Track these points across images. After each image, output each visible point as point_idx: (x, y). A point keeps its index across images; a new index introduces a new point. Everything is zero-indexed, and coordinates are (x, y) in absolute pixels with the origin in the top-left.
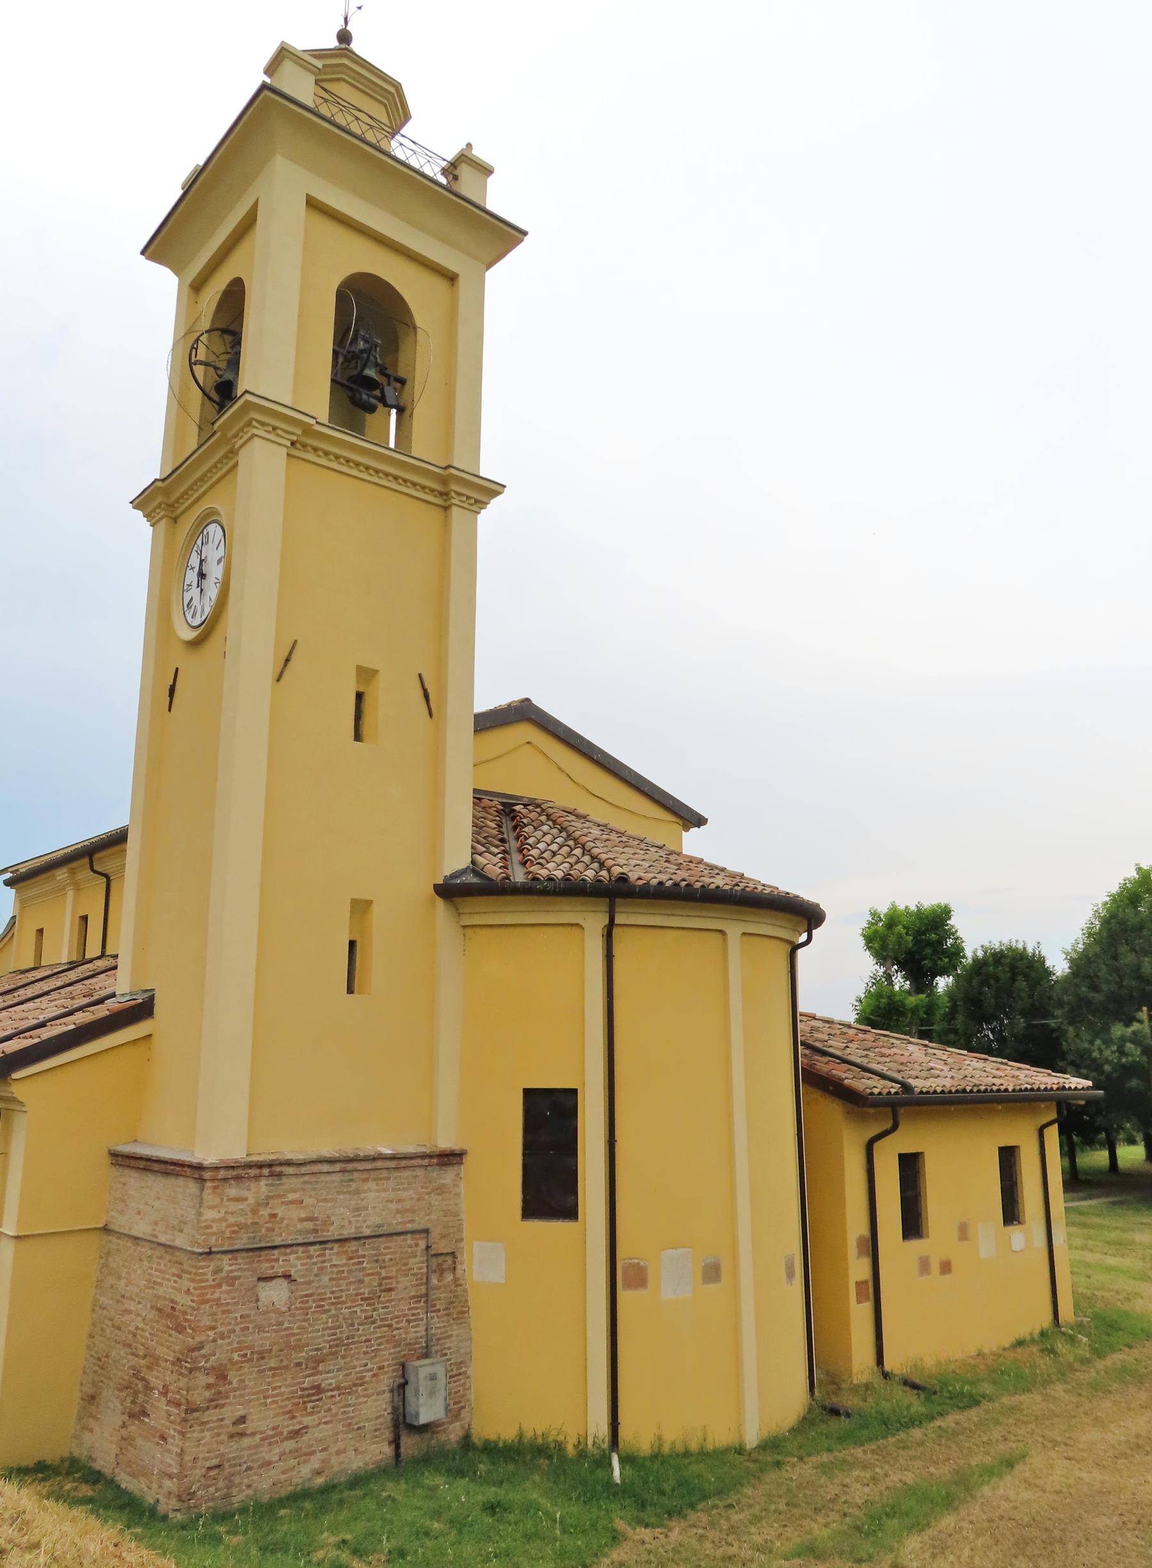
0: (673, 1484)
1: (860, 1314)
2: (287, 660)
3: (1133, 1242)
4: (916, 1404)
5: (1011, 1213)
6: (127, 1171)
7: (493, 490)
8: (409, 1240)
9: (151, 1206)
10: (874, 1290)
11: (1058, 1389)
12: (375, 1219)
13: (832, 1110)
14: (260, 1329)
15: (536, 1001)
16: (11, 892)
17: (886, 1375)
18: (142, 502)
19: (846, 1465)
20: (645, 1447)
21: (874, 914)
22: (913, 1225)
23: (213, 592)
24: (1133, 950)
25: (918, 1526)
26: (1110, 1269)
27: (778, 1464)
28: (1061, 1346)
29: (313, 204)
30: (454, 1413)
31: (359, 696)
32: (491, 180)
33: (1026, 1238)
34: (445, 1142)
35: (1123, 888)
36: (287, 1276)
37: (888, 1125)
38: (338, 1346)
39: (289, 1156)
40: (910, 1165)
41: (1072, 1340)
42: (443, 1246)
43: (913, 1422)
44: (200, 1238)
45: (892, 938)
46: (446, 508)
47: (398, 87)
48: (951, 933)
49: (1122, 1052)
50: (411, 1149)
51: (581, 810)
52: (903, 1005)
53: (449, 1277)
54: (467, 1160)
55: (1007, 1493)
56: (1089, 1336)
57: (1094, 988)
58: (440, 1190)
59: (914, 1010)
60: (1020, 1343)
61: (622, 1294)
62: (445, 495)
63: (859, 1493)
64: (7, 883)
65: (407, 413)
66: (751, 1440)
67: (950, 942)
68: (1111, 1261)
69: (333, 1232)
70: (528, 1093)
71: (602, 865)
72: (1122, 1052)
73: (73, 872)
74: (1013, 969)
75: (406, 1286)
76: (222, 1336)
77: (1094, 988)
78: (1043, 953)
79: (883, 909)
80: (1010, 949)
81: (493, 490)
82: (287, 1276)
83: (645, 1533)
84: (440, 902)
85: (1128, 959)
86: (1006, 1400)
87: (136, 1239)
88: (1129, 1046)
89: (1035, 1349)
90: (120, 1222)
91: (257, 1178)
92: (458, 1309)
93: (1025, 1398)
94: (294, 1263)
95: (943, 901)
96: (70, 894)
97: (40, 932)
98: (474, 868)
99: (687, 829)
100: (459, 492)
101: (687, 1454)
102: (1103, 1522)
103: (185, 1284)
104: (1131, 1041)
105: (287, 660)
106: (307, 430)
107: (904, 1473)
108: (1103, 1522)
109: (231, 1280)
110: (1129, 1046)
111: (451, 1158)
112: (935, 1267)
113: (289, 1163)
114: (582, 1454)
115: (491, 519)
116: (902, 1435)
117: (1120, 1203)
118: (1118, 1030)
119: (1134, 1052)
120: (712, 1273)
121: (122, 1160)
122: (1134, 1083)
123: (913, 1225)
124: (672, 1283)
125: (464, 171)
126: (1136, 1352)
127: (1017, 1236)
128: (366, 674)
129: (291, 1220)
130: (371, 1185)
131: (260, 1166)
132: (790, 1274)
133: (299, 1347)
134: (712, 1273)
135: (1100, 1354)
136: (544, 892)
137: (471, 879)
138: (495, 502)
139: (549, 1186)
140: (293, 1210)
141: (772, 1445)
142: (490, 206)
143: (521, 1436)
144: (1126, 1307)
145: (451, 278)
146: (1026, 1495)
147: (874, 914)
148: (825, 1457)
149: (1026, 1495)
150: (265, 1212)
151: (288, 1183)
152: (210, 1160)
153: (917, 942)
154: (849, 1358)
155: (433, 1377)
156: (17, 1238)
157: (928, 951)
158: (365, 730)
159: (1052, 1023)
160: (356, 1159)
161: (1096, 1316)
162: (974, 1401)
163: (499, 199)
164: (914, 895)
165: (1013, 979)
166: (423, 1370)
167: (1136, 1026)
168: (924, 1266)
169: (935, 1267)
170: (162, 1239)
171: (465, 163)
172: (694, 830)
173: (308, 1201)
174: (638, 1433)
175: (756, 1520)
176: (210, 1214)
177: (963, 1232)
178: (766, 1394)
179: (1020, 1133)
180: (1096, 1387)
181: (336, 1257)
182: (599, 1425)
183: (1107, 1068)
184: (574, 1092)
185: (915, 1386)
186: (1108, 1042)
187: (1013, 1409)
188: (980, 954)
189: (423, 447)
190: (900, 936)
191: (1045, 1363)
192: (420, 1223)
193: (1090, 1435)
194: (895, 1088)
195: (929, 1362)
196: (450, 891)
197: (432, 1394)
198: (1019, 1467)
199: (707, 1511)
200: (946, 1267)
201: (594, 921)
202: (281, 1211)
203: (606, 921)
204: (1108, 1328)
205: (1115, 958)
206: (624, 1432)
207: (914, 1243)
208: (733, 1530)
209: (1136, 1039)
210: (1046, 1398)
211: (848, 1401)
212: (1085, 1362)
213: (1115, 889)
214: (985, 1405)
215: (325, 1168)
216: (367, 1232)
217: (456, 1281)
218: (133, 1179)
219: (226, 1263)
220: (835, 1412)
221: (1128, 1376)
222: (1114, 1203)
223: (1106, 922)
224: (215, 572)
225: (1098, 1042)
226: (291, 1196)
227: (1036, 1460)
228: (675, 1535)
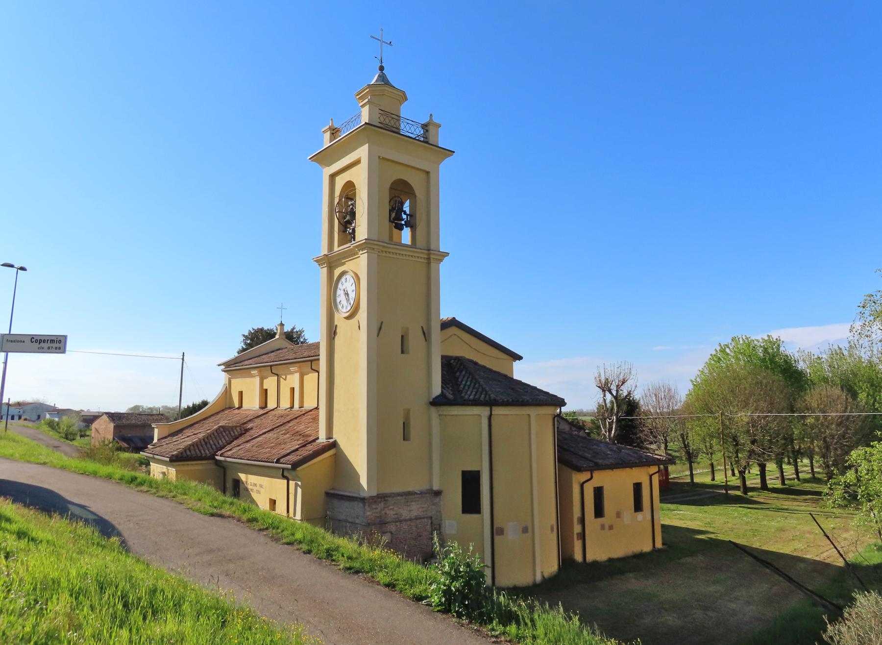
2: (380, 329)
5: (638, 507)
10: (583, 536)
12: (415, 514)
33: (643, 517)
34: (436, 488)
37: (589, 477)
61: (497, 538)
70: (65, 337)
73: (260, 371)
98: (443, 395)
105: (380, 329)
111: (438, 493)
112: (607, 527)
120: (525, 530)
123: (599, 512)
124: (512, 535)
127: (640, 516)
131: (381, 498)
132: (552, 530)
134: (525, 530)
139: (471, 504)
142: (515, 378)
168: (603, 527)
169: (607, 527)
176: (368, 513)
177: (618, 515)
184: (478, 472)
189: (421, 242)
192: (430, 515)
196: (436, 402)
202: (388, 512)
207: (599, 520)
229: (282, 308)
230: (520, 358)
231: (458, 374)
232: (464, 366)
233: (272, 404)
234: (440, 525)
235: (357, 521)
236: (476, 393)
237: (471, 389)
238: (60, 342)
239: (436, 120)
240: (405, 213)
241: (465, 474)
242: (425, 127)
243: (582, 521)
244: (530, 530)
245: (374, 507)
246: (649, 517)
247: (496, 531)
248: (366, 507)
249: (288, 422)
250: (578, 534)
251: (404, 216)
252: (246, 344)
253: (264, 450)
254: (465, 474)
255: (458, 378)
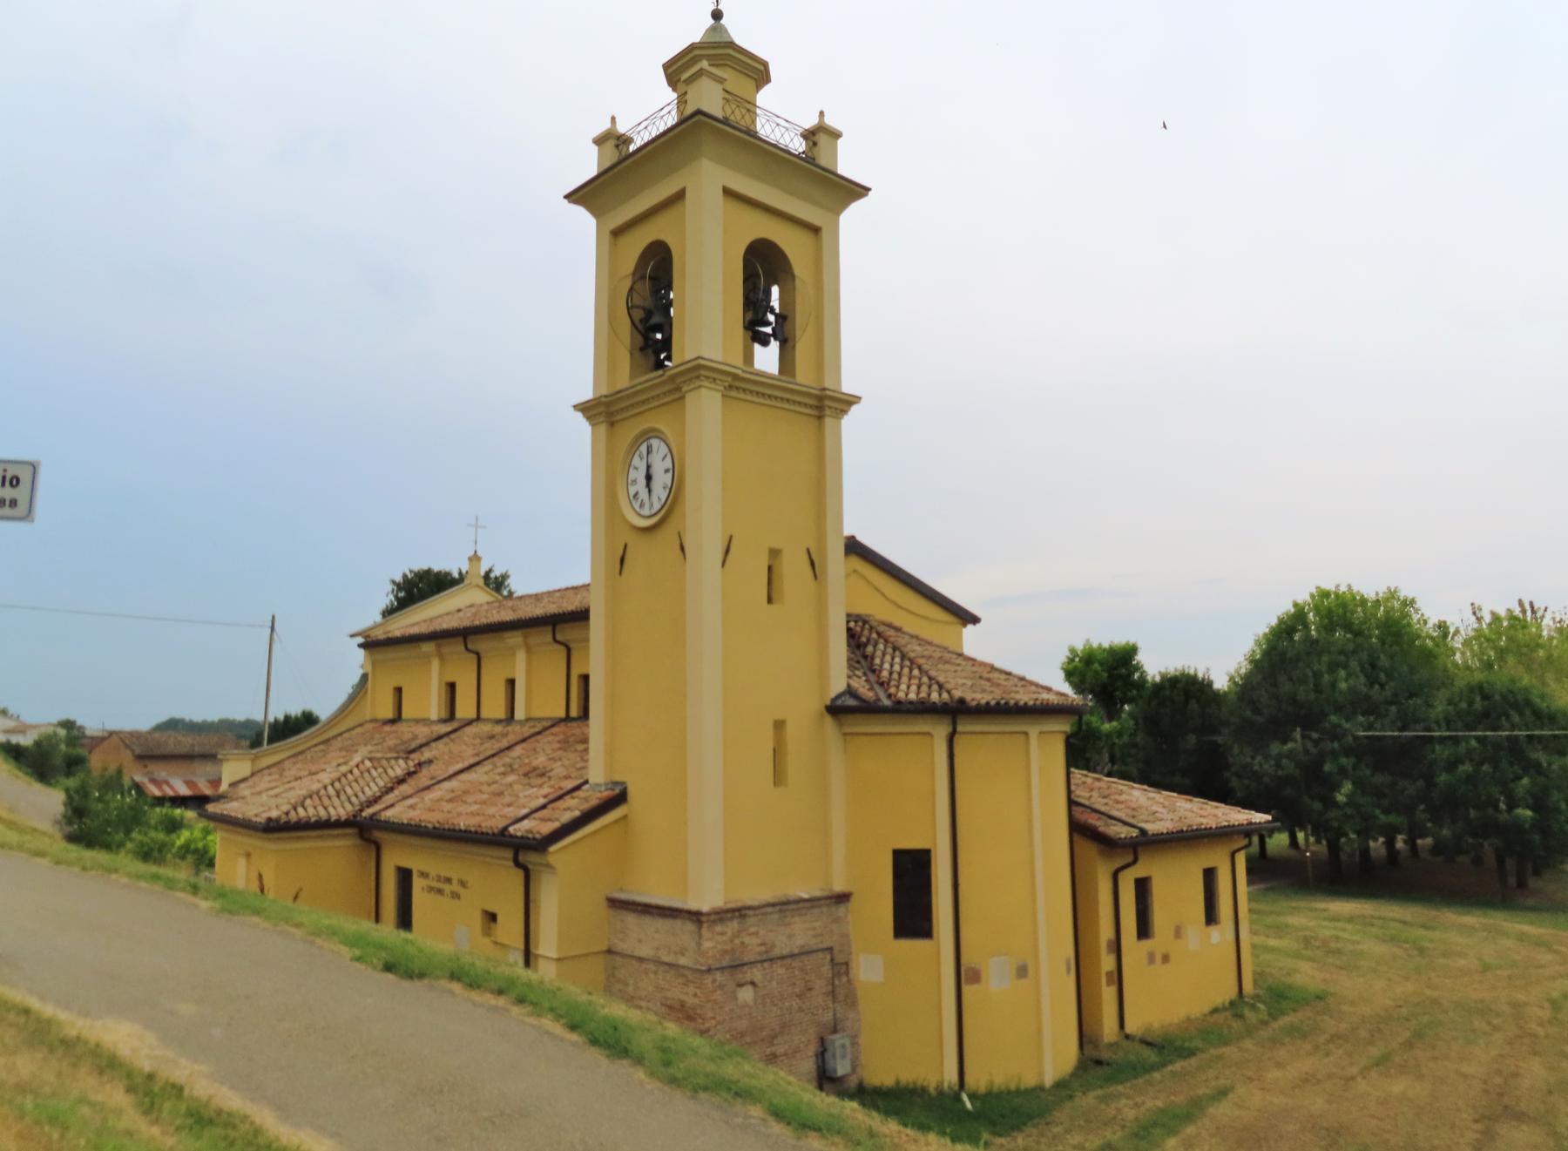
0: (1008, 1110)
1: (1108, 994)
2: (727, 551)
3: (1287, 926)
4: (1150, 1056)
5: (1211, 917)
6: (625, 913)
7: (849, 401)
8: (820, 955)
9: (644, 937)
10: (1118, 978)
11: (1248, 1043)
13: (1088, 849)
14: (740, 1017)
15: (903, 793)
16: (362, 652)
17: (1127, 1037)
18: (585, 409)
19: (1119, 1096)
20: (982, 1089)
21: (1072, 651)
22: (1144, 930)
23: (660, 493)
24: (1290, 679)
25: (1172, 1132)
26: (1272, 950)
27: (1071, 1097)
28: (1247, 1012)
29: (728, 192)
30: (854, 1068)
31: (770, 568)
32: (840, 142)
33: (1221, 934)
34: (839, 887)
35: (1281, 621)
36: (753, 984)
37: (1130, 859)
38: (785, 1027)
39: (749, 903)
40: (1142, 886)
41: (1253, 1007)
42: (840, 958)
43: (1154, 1068)
44: (702, 960)
45: (1089, 675)
46: (820, 418)
47: (765, 65)
48: (1138, 668)
49: (1278, 766)
50: (818, 893)
51: (897, 623)
52: (1099, 731)
53: (844, 979)
54: (853, 899)
55: (1222, 1111)
56: (1264, 1003)
57: (1257, 711)
58: (837, 920)
59: (1109, 735)
60: (1215, 1011)
61: (966, 989)
62: (820, 408)
63: (1130, 1114)
64: (360, 646)
65: (789, 344)
66: (1048, 1081)
67: (1136, 676)
68: (1272, 942)
69: (777, 952)
71: (941, 686)
72: (1278, 766)
73: (439, 646)
74: (1186, 691)
75: (820, 986)
76: (719, 1023)
77: (1257, 711)
78: (1212, 677)
79: (1079, 647)
80: (1183, 674)
81: (849, 401)
82: (753, 984)
83: (1002, 1140)
84: (828, 719)
85: (1286, 687)
86: (1213, 1051)
87: (641, 959)
88: (1285, 761)
89: (1228, 1014)
90: (621, 946)
91: (731, 919)
92: (851, 1000)
93: (1225, 1050)
94: (756, 974)
95: (1132, 641)
96: (435, 664)
97: (399, 691)
98: (850, 691)
99: (965, 625)
100: (827, 405)
101: (1009, 1092)
102: (1291, 1128)
103: (692, 989)
104: (1288, 757)
105: (727, 551)
106: (735, 377)
107: (1153, 1102)
108: (1291, 1128)
109: (721, 987)
110: (1285, 761)
111: (843, 898)
112: (1159, 958)
113: (750, 908)
114: (941, 1093)
115: (851, 424)
116: (1147, 1077)
117: (1272, 889)
118: (1275, 748)
119: (1289, 767)
120: (1022, 972)
121: (614, 903)
122: (1288, 791)
123: (1144, 930)
124: (996, 981)
125: (822, 139)
126: (1300, 1015)
128: (775, 553)
129: (752, 944)
130: (797, 919)
131: (733, 910)
132: (1069, 970)
133: (762, 1029)
135: (1274, 1017)
136: (908, 712)
137: (851, 702)
138: (854, 408)
139: (912, 917)
140: (753, 939)
141: (1060, 1085)
142: (841, 171)
143: (898, 1083)
144: (1288, 980)
145: (815, 230)
146: (1237, 1113)
147: (1072, 651)
148: (1100, 1092)
149: (1237, 1113)
150: (737, 941)
151: (751, 921)
152: (705, 908)
153: (1110, 676)
154: (1101, 1026)
155: (843, 1046)
156: (559, 960)
157: (1119, 683)
158: (774, 596)
159: (1220, 739)
160: (788, 903)
161: (1270, 989)
162: (1192, 1053)
163: (848, 164)
164: (1107, 637)
165: (1187, 702)
166: (838, 1040)
167: (1290, 745)
168: (1151, 958)
169: (1159, 958)
170: (666, 959)
171: (819, 135)
172: (970, 627)
173: (762, 932)
174: (978, 1079)
175: (1068, 1131)
177: (1178, 933)
178: (1057, 1056)
179: (1218, 858)
180: (1275, 1042)
181: (779, 970)
182: (951, 1075)
183: (1266, 780)
185: (1148, 1044)
186: (1267, 757)
187: (1220, 1057)
188: (1158, 679)
189: (804, 375)
190: (1096, 672)
191: (1236, 1025)
193: (1273, 1074)
194: (1135, 833)
195: (1156, 1025)
196: (835, 710)
197: (844, 1057)
198: (1230, 1096)
199: (1034, 1126)
200: (1166, 959)
201: (940, 731)
202: (747, 940)
203: (950, 729)
204: (1279, 998)
205: (1275, 685)
206: (969, 1079)
208: (1055, 1137)
209: (1291, 755)
210: (1240, 1049)
211: (1105, 1055)
212: (1264, 1023)
213: (1274, 622)
214: (1200, 1056)
215: (770, 909)
216: (796, 951)
217: (849, 981)
218: (631, 919)
219: (719, 977)
220: (1099, 1063)
221: (1295, 1032)
222: (1266, 889)
223: (1267, 654)
224: (661, 480)
225: (1259, 758)
226: (753, 930)
227: (1241, 1090)
228: (1020, 1141)
229: (476, 526)
230: (975, 620)
231: (870, 649)
232: (879, 634)
233: (465, 709)
234: (847, 964)
235: (683, 961)
236: (919, 687)
237: (905, 679)
238: (15, 482)
239: (830, 121)
240: (772, 311)
241: (898, 855)
242: (810, 135)
243: (1117, 947)
244: (1031, 971)
245: (719, 928)
246: (1231, 936)
247: (963, 976)
248: (705, 931)
249: (509, 748)
250: (1109, 974)
251: (771, 318)
252: (397, 598)
253: (462, 808)
254: (898, 855)
255: (873, 658)
